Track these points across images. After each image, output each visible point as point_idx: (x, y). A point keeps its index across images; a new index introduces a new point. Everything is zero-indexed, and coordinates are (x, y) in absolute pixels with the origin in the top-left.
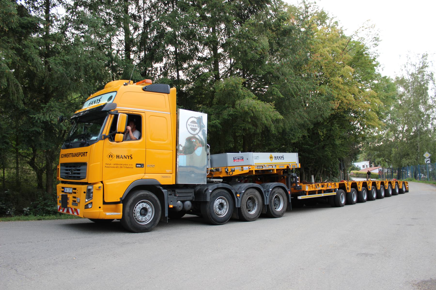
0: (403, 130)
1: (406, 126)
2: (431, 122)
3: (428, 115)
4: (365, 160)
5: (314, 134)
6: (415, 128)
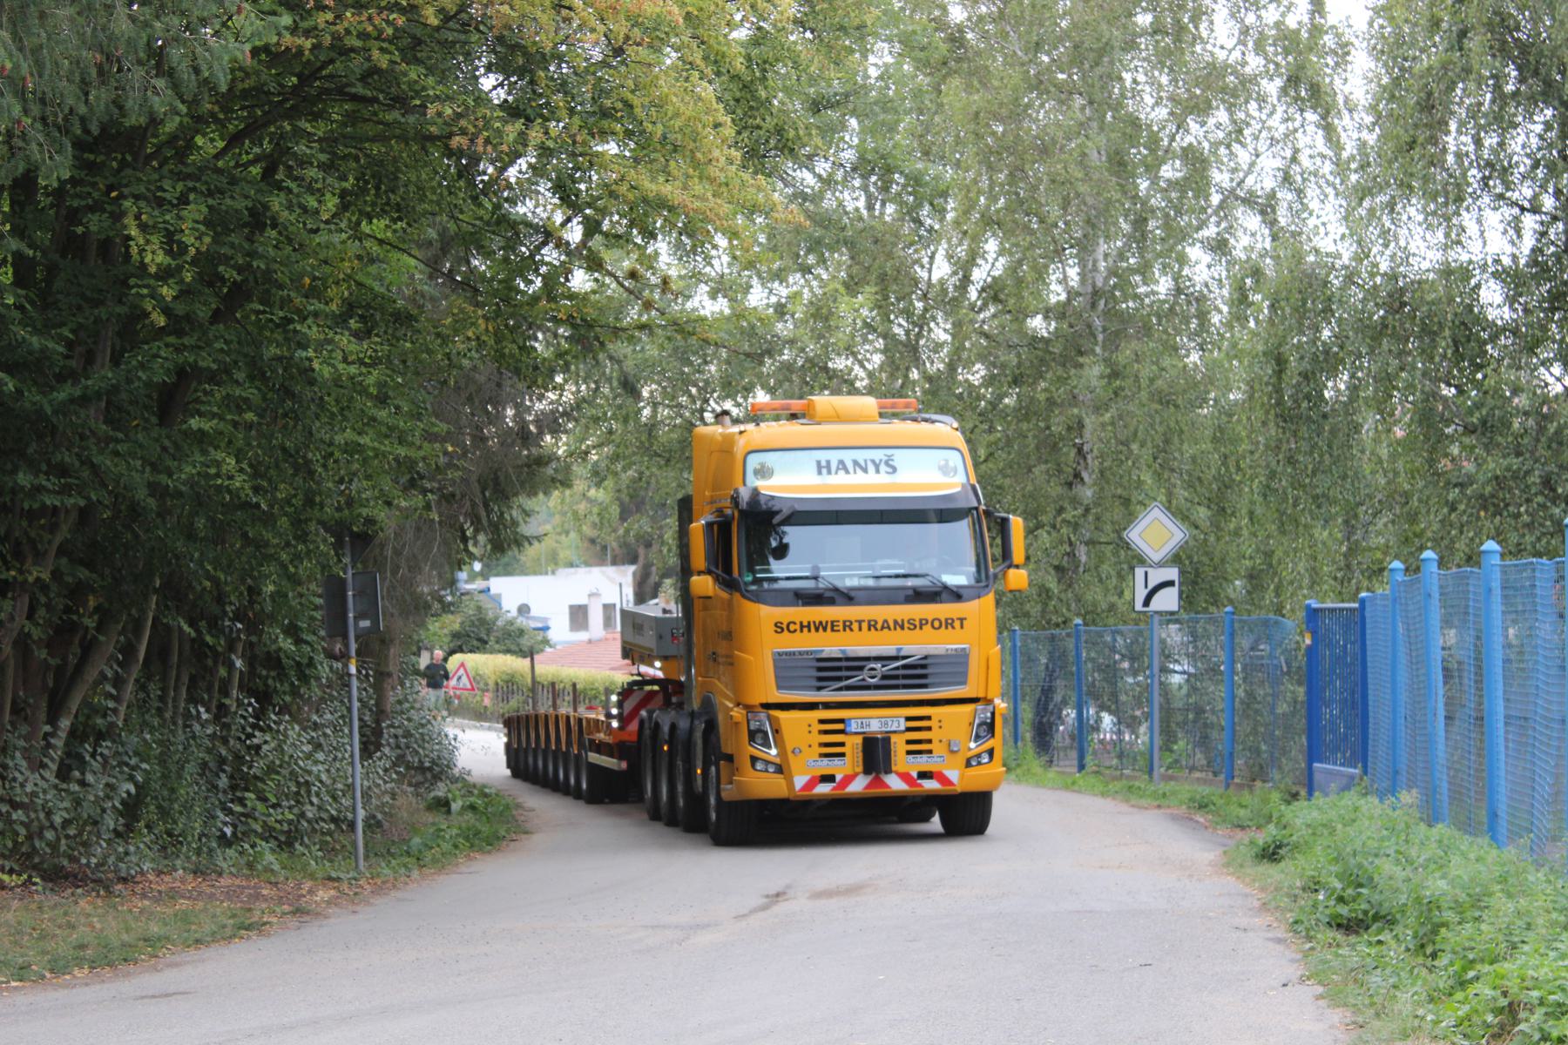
0: (966, 280)
1: (991, 246)
2: (1211, 231)
3: (1197, 162)
4: (599, 553)
5: (72, 245)
6: (1073, 273)
